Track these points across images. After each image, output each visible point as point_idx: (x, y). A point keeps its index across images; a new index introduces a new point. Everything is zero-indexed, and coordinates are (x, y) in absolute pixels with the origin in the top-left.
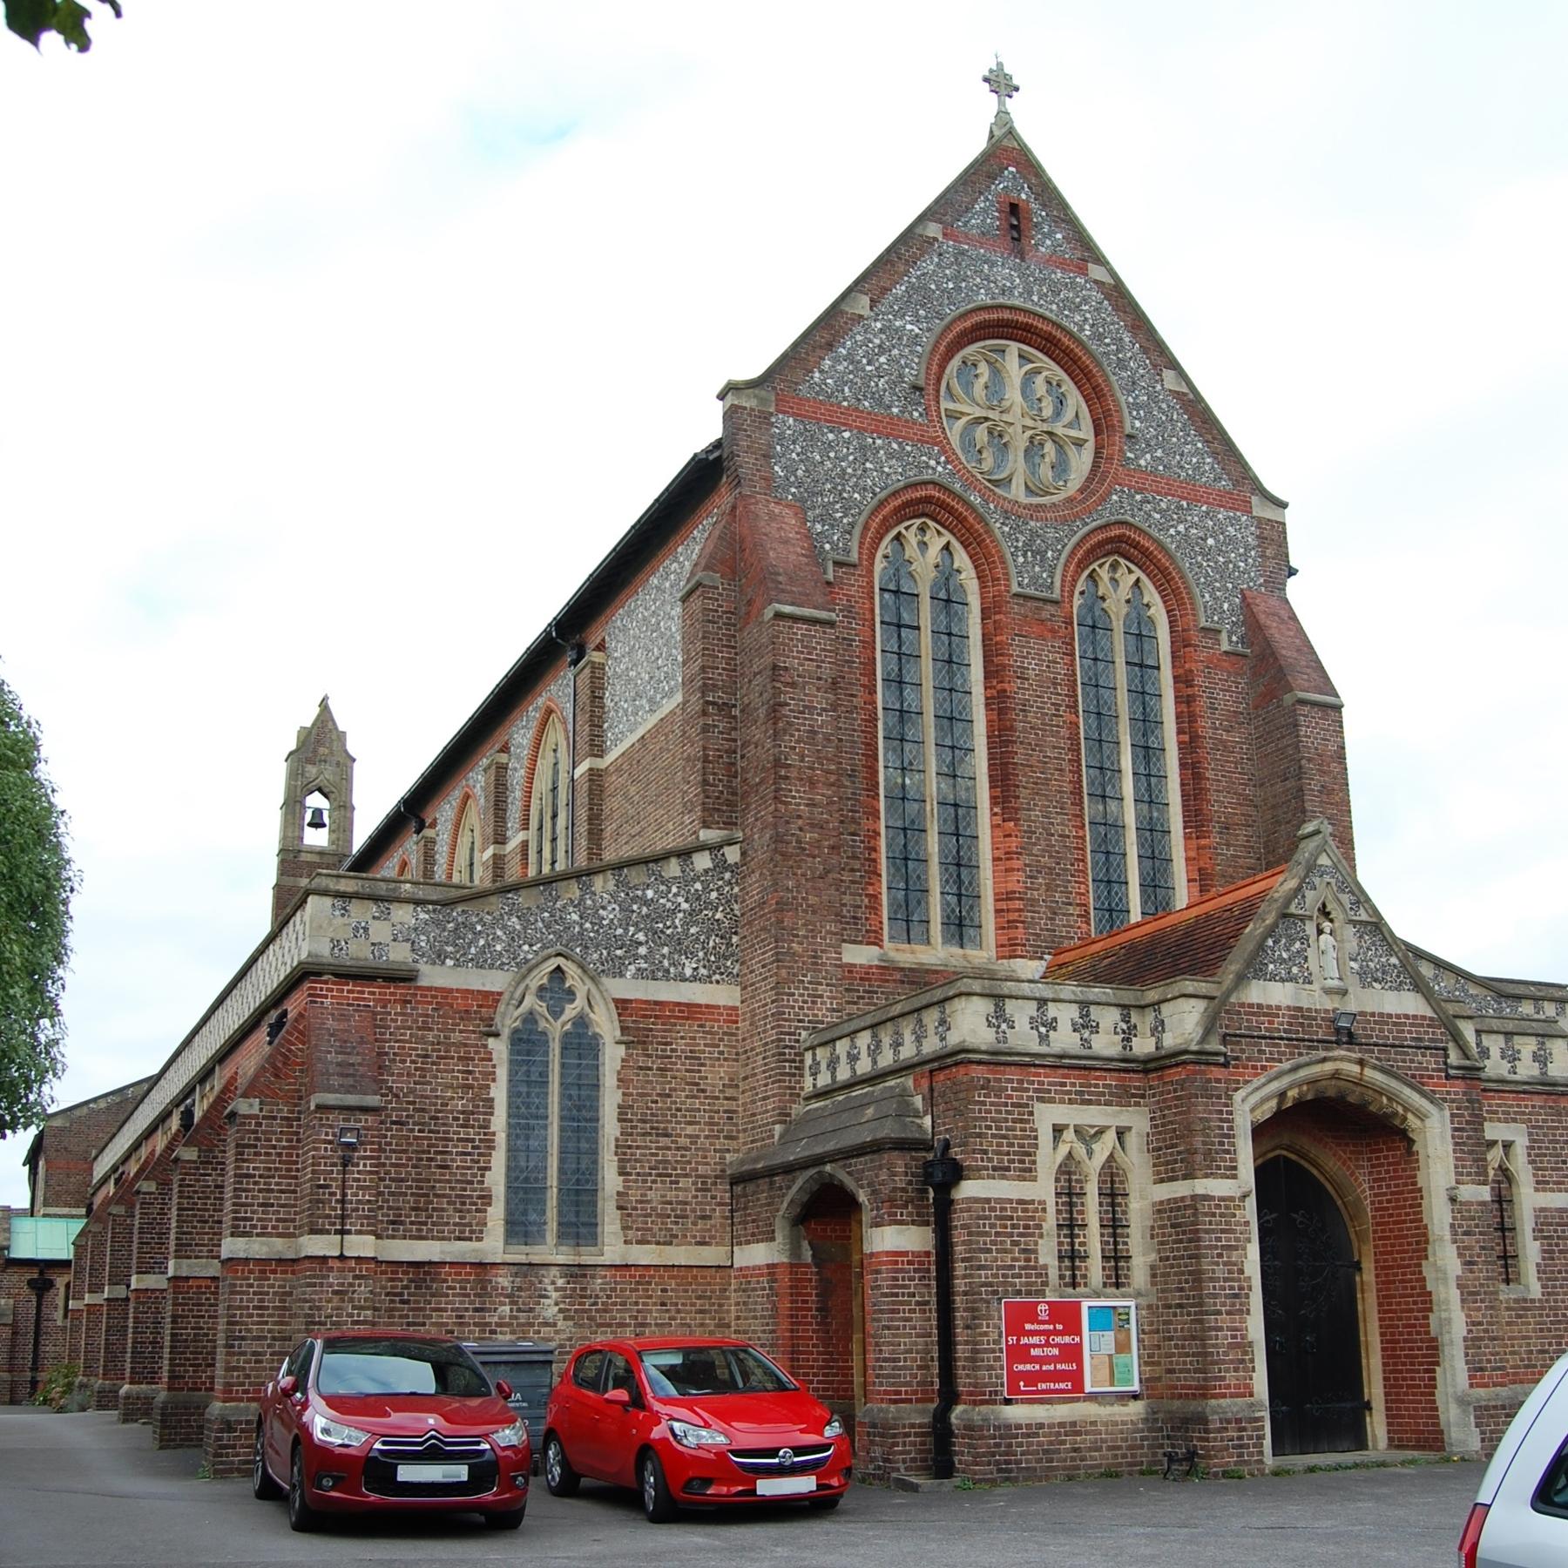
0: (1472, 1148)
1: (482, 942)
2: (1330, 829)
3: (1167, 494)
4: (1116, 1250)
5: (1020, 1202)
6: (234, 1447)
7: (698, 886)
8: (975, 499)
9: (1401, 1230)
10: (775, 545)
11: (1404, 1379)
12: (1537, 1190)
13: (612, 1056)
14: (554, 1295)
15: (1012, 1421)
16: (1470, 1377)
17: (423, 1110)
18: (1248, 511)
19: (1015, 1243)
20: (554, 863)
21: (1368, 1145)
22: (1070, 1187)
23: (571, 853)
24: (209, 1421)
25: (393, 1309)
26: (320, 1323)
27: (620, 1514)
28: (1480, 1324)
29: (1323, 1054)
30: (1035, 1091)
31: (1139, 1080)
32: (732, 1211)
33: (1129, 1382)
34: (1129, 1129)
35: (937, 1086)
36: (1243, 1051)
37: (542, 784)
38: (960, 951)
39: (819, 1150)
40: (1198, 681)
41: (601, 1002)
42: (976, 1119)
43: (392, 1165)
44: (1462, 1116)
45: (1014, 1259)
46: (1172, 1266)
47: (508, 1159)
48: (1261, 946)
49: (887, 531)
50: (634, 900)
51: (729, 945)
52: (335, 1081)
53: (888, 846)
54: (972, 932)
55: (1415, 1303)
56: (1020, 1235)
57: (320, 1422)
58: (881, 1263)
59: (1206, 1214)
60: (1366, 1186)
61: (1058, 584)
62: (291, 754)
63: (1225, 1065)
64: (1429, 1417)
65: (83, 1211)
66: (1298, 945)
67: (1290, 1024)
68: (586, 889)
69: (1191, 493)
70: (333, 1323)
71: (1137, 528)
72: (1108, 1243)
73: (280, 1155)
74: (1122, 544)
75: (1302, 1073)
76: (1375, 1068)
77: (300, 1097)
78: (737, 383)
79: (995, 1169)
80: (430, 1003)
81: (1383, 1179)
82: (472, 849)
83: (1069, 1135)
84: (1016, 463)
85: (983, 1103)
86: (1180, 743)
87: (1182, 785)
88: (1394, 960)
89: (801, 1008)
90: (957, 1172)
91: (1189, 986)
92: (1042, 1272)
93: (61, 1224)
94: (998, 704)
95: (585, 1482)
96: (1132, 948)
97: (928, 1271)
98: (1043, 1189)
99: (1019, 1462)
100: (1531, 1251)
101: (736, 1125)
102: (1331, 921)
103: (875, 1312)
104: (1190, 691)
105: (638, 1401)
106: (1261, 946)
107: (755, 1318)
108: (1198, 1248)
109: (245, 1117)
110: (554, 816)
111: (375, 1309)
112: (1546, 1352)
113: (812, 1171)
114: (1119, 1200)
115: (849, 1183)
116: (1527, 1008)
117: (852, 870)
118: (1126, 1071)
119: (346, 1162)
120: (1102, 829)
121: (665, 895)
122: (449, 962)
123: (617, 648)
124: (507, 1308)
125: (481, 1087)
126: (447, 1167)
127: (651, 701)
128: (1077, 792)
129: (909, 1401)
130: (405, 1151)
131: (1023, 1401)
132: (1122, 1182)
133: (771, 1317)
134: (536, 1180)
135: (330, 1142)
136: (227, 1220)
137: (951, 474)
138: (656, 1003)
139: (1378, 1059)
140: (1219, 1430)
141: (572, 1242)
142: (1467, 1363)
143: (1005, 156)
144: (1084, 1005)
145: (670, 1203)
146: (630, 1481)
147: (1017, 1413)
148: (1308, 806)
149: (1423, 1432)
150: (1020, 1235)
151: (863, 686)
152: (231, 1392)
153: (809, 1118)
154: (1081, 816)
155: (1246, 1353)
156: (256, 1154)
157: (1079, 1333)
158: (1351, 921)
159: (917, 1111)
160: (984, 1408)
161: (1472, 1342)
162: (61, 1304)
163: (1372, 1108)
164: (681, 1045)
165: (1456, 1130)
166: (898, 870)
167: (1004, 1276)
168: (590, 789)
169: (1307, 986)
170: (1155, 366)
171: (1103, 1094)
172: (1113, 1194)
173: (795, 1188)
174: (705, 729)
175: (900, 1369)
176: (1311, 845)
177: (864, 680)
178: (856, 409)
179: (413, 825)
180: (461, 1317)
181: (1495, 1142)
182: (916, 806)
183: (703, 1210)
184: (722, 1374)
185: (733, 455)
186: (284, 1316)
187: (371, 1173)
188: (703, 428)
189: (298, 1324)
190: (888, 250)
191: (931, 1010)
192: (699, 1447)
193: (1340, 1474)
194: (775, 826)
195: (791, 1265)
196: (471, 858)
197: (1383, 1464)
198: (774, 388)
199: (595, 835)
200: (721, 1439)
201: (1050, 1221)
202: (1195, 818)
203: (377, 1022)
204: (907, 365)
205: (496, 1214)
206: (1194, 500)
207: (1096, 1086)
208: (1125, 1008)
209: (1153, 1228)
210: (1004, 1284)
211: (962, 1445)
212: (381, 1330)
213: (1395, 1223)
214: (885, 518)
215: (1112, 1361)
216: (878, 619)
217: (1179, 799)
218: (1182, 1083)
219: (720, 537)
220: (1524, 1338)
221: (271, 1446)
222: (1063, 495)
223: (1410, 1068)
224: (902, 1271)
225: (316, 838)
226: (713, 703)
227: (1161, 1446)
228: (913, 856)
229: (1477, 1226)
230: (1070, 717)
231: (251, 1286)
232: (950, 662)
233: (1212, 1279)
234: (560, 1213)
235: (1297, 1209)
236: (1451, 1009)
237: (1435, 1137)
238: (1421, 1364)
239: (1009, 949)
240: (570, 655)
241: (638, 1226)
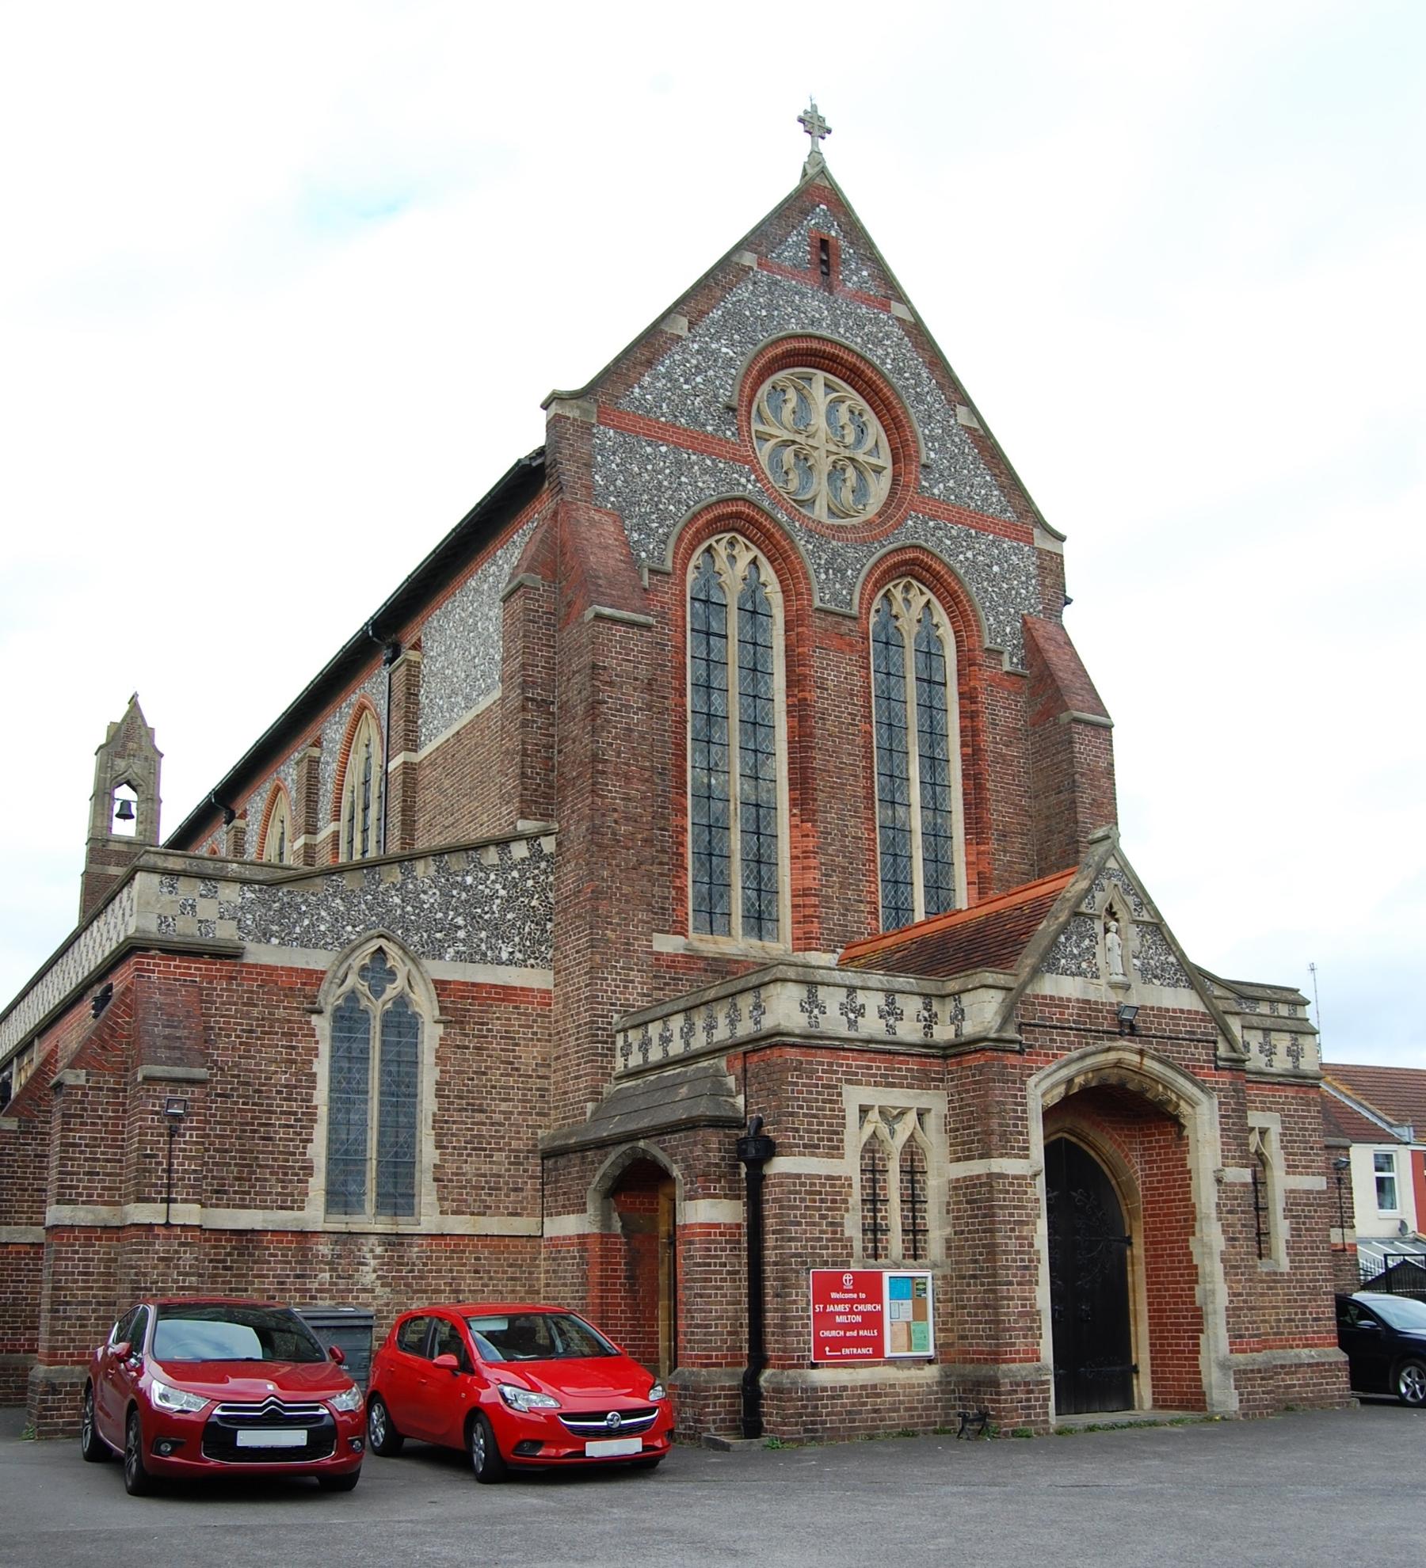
0: (1236, 1131)
1: (306, 922)
3: (957, 523)
4: (914, 1224)
6: (58, 1409)
7: (515, 874)
8: (782, 517)
9: (1169, 1208)
10: (596, 550)
11: (1169, 1345)
12: (1288, 1173)
13: (431, 1034)
14: (373, 1262)
15: (818, 1384)
16: (1231, 1344)
17: (248, 1084)
18: (1030, 542)
19: (823, 1217)
20: (364, 852)
21: (1141, 1129)
22: (874, 1165)
23: (383, 843)
24: (33, 1383)
25: (216, 1276)
26: (146, 1289)
27: (446, 1474)
28: (1240, 1295)
29: (1108, 1044)
30: (844, 1073)
31: (939, 1065)
32: (543, 1184)
33: (925, 1347)
34: (929, 1110)
35: (751, 1067)
36: (1036, 1040)
37: (354, 778)
38: (759, 943)
39: (632, 1126)
40: (981, 698)
41: (421, 983)
42: (789, 1099)
43: (216, 1136)
44: (1228, 1104)
45: (821, 1232)
46: (967, 1240)
47: (330, 1132)
48: (1054, 942)
49: (700, 543)
50: (454, 885)
51: (544, 931)
52: (163, 1054)
54: (770, 925)
55: (1182, 1275)
56: (829, 1209)
57: (157, 1388)
59: (1000, 1192)
60: (1138, 1167)
61: (856, 601)
62: (101, 747)
63: (1020, 1052)
64: (1192, 1380)
66: (1087, 942)
67: (1079, 1015)
68: (408, 873)
69: (980, 523)
70: (158, 1289)
71: (929, 552)
72: (906, 1217)
73: (106, 1125)
75: (1089, 1062)
76: (1153, 1058)
77: (124, 1069)
78: (562, 393)
79: (805, 1146)
80: (256, 980)
81: (1155, 1161)
82: (282, 840)
83: (874, 1115)
84: (820, 486)
85: (796, 1084)
86: (963, 755)
87: (965, 794)
88: (1172, 959)
89: (614, 992)
90: (770, 1150)
91: (989, 978)
92: (847, 1245)
94: (799, 711)
95: (407, 1442)
96: (923, 943)
97: (739, 1242)
98: (849, 1166)
99: (824, 1422)
100: (1281, 1229)
101: (548, 1102)
102: (1117, 920)
103: (687, 1281)
104: (974, 707)
105: (467, 1365)
106: (1054, 942)
107: (565, 1285)
108: (993, 1223)
109: (72, 1087)
110: (366, 808)
111: (200, 1275)
112: (1293, 1320)
113: (625, 1147)
114: (918, 1177)
115: (663, 1158)
116: (1264, 1008)
117: (661, 863)
118: (927, 1056)
119: (173, 1133)
120: (890, 833)
121: (483, 882)
122: (275, 941)
123: (433, 647)
124: (327, 1275)
125: (304, 1062)
126: (270, 1139)
127: (467, 698)
128: (870, 797)
129: (720, 1365)
130: (229, 1123)
131: (829, 1366)
132: (921, 1161)
133: (581, 1284)
134: (356, 1152)
135: (157, 1113)
136: (52, 1188)
137: (761, 492)
138: (474, 985)
139: (1156, 1050)
140: (1010, 1393)
141: (390, 1212)
142: (1228, 1330)
143: (817, 194)
144: (890, 993)
145: (485, 1176)
146: (458, 1442)
147: (823, 1376)
148: (1080, 817)
149: (1186, 1394)
150: (829, 1209)
151: (676, 689)
152: (55, 1355)
153: (621, 1097)
154: (873, 820)
155: (1034, 1321)
156: (82, 1124)
157: (880, 1301)
158: (1135, 922)
159: (730, 1090)
160: (791, 1372)
161: (1233, 1312)
163: (1149, 1095)
165: (1222, 1116)
166: (702, 865)
167: (813, 1247)
168: (404, 782)
169: (1095, 981)
170: (949, 402)
171: (906, 1078)
172: (913, 1172)
173: (607, 1163)
174: (525, 724)
175: (712, 1334)
177: (675, 684)
178: (673, 425)
179: (223, 816)
180: (282, 1283)
181: (1253, 1129)
182: (720, 805)
183: (516, 1183)
184: (542, 1339)
186: (109, 1282)
187: (197, 1143)
188: (527, 436)
189: (123, 1289)
190: (707, 276)
191: (746, 995)
192: (531, 1411)
193: (1117, 1432)
194: (592, 818)
195: (602, 1236)
196: (281, 847)
197: (1153, 1424)
198: (596, 401)
199: (408, 826)
200: (552, 1403)
201: (856, 1196)
202: (976, 826)
203: (203, 998)
204: (722, 386)
205: (317, 1184)
206: (983, 529)
207: (900, 1070)
209: (948, 1204)
211: (769, 1406)
212: (205, 1296)
213: (1165, 1201)
214: (698, 530)
215: (909, 1328)
216: (689, 627)
217: (961, 808)
218: (980, 1069)
219: (542, 541)
220: (1274, 1307)
221: (101, 1408)
222: (862, 518)
223: (1184, 1059)
224: (714, 1242)
225: (125, 829)
226: (532, 700)
227: (953, 1407)
228: (717, 852)
229: (1239, 1205)
231: (77, 1252)
232: (755, 670)
233: (1005, 1252)
234: (378, 1185)
235: (1079, 1187)
236: (1221, 1005)
237: (1204, 1122)
238: (1186, 1331)
239: (804, 942)
240: (386, 653)
241: (453, 1200)
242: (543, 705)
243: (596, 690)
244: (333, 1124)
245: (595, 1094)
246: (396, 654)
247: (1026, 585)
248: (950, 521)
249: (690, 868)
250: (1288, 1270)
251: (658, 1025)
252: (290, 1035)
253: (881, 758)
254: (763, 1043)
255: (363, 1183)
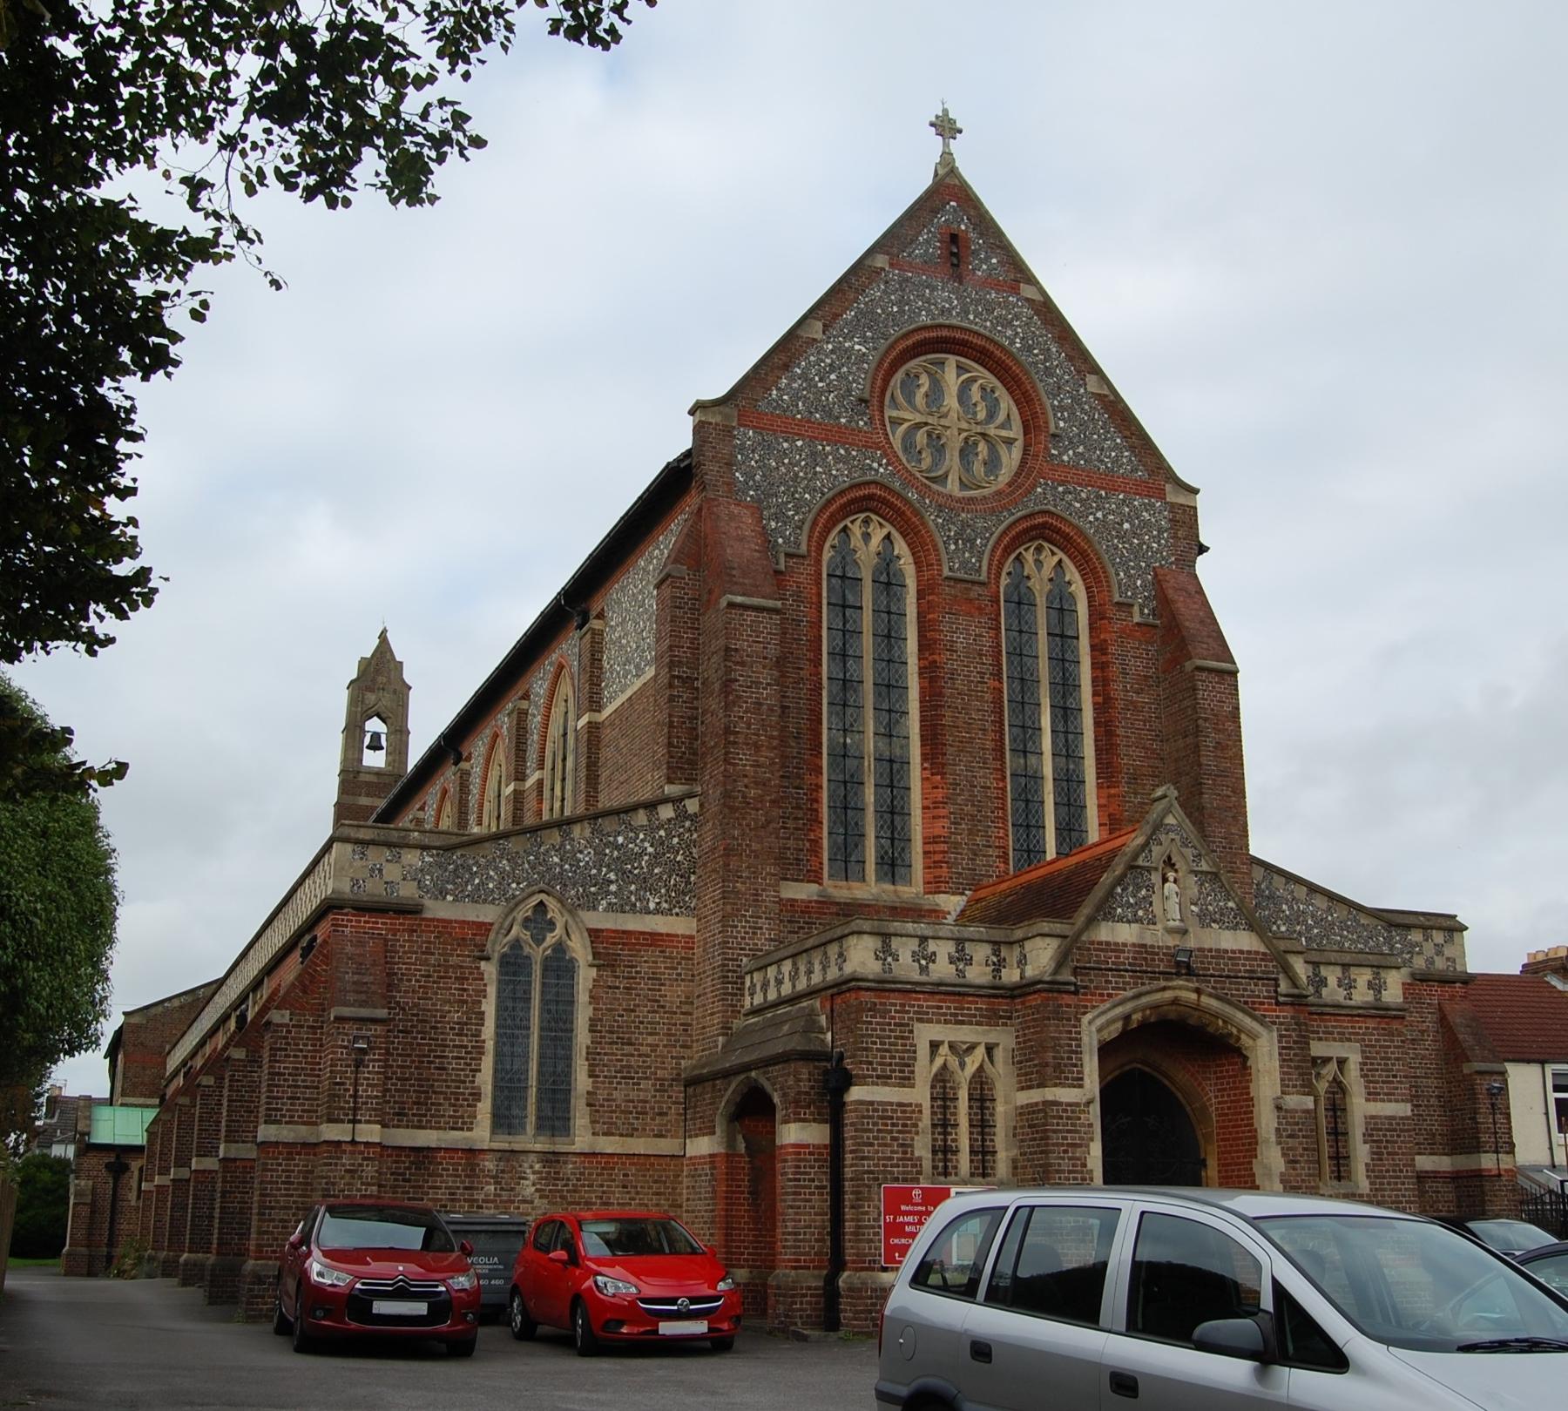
0: (1301, 1066)
2: (1176, 793)
5: (900, 1104)
7: (662, 833)
8: (912, 495)
12: (1367, 1100)
14: (532, 1177)
18: (1162, 497)
19: (894, 1139)
29: (1163, 983)
36: (1091, 981)
38: (892, 887)
48: (1111, 893)
49: (834, 525)
51: (688, 882)
52: (351, 997)
53: (830, 797)
57: (316, 1268)
58: (788, 1153)
61: (985, 568)
63: (1076, 993)
65: (157, 1101)
66: (1144, 892)
68: (567, 836)
69: (1110, 482)
74: (1044, 530)
75: (1144, 1000)
76: (1210, 995)
79: (878, 1077)
83: (944, 1049)
84: (952, 460)
86: (1095, 704)
87: (1096, 740)
90: (847, 1081)
91: (1045, 927)
93: (137, 1112)
94: (929, 672)
95: (542, 1329)
98: (920, 1094)
100: (1361, 1153)
105: (575, 1258)
106: (1111, 893)
110: (564, 759)
113: (743, 1076)
114: (988, 1104)
119: (359, 1064)
120: (1023, 781)
121: (633, 841)
122: (449, 898)
125: (474, 1002)
127: (637, 666)
137: (892, 474)
138: (624, 932)
148: (1204, 760)
154: (1002, 770)
158: (1192, 872)
160: (863, 1274)
162: (135, 1186)
163: (1211, 1029)
164: (644, 968)
170: (1079, 372)
172: (982, 1097)
174: (671, 699)
176: (1160, 806)
177: (810, 655)
178: (809, 421)
182: (856, 762)
185: (699, 464)
188: (678, 440)
190: (840, 281)
194: (725, 784)
195: (727, 1155)
199: (592, 780)
200: (633, 1290)
201: (926, 1121)
203: (387, 949)
205: (484, 1108)
208: (996, 945)
210: (884, 1172)
214: (832, 514)
216: (825, 602)
217: (1093, 753)
218: (1037, 1007)
222: (994, 489)
225: (374, 760)
226: (678, 677)
230: (993, 683)
233: (1058, 1172)
236: (1282, 945)
237: (1266, 1055)
239: (935, 885)
241: (604, 1122)
242: (688, 681)
243: (729, 670)
244: (499, 1055)
245: (726, 1029)
246: (585, 621)
247: (1157, 539)
248: (1080, 485)
249: (825, 822)
250: (1367, 1191)
251: (774, 967)
252: (462, 979)
253: (1012, 711)
254: (844, 987)
255: (525, 1108)
